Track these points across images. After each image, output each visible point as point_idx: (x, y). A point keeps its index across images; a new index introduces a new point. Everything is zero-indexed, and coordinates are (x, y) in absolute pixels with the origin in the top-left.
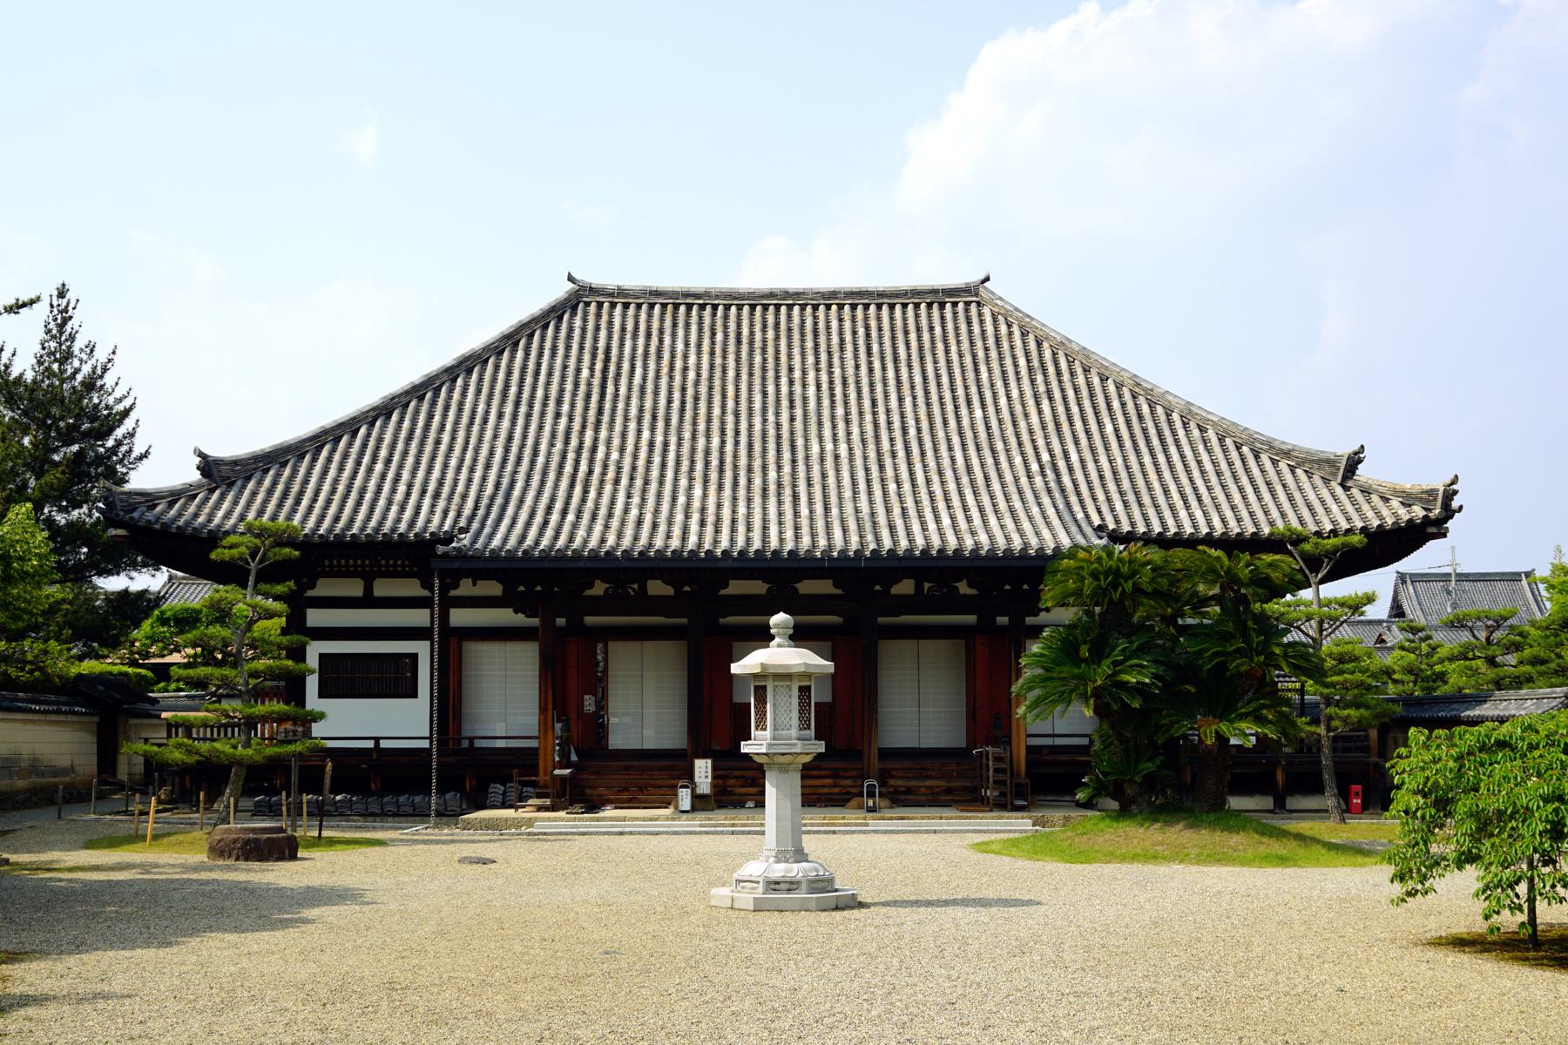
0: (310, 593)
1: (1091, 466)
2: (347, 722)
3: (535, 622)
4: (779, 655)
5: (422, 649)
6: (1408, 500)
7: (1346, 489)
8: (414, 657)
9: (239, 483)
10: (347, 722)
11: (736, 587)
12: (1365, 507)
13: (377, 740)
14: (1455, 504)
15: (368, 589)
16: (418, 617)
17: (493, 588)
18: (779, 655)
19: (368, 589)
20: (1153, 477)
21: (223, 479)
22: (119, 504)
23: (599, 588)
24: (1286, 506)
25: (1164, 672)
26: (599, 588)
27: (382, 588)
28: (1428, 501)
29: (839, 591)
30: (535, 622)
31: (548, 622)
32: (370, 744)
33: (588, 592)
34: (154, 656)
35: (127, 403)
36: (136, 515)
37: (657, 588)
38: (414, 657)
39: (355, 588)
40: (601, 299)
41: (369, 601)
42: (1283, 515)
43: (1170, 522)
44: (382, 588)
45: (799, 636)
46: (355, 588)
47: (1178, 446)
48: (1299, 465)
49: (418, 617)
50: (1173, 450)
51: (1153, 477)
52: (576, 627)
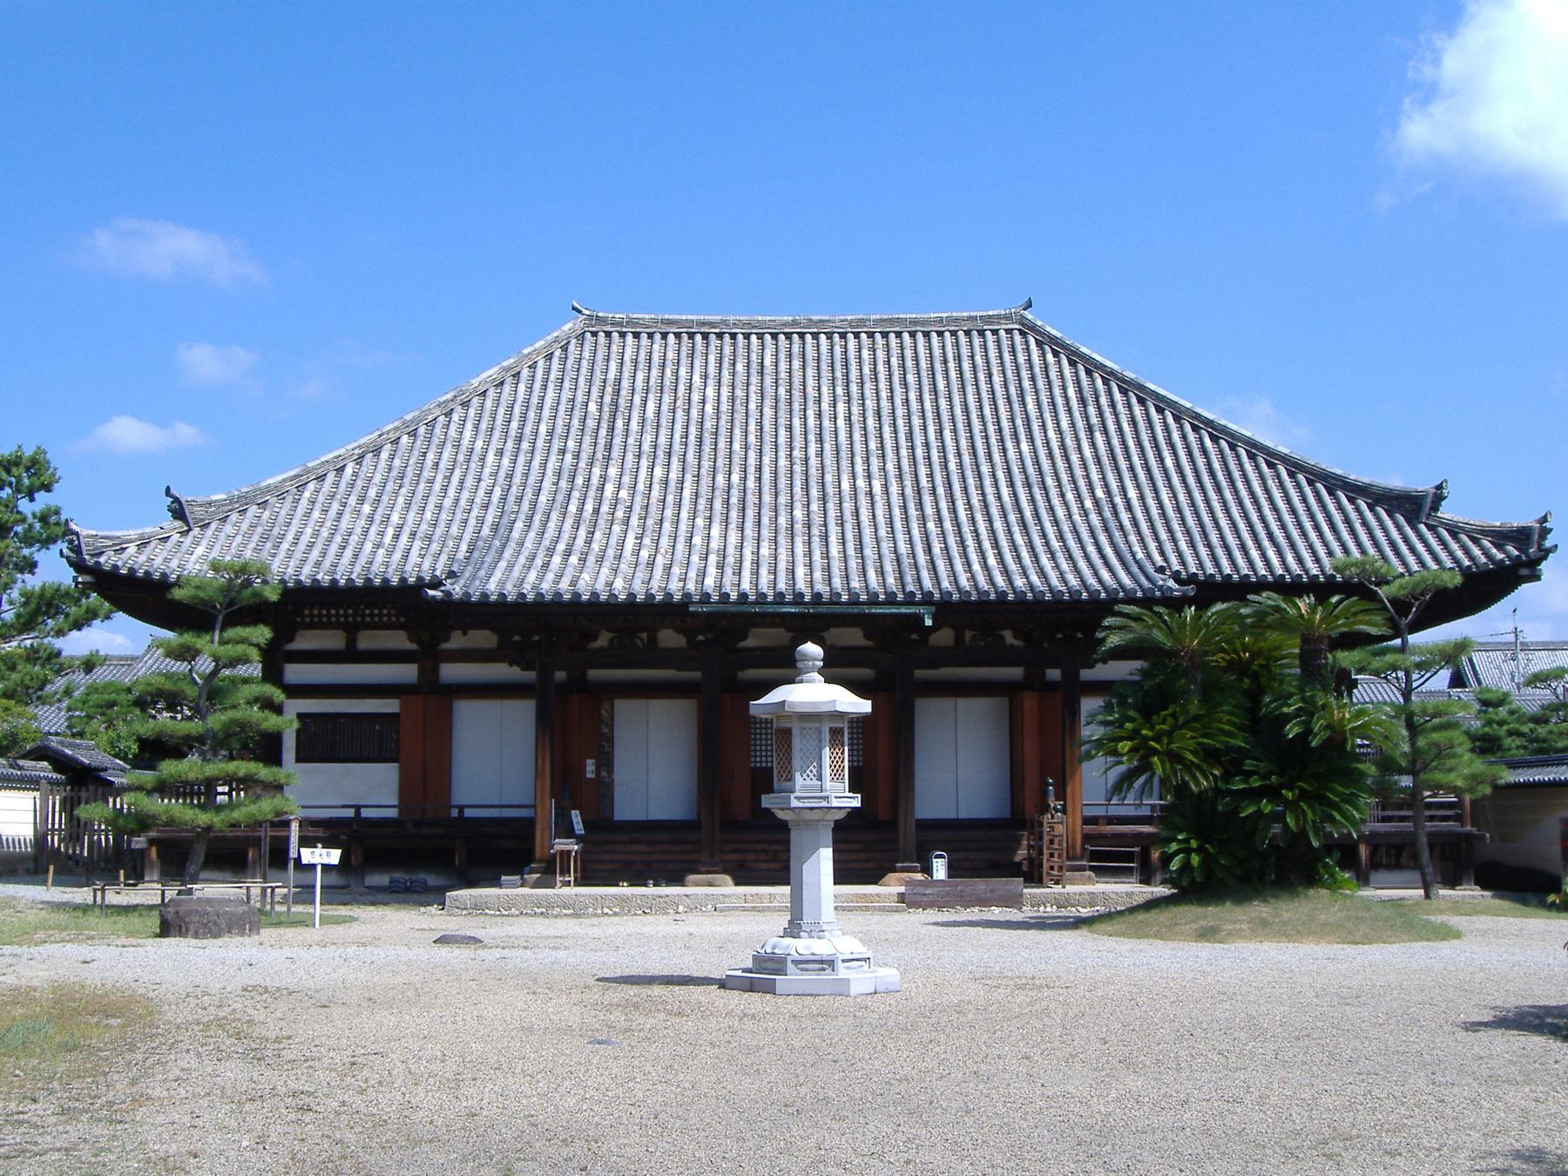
3: (531, 675)
4: (814, 692)
6: (1501, 537)
7: (1431, 528)
9: (213, 526)
12: (1454, 546)
13: (358, 808)
14: (1548, 544)
15: (351, 643)
16: (407, 672)
17: (484, 638)
18: (814, 692)
19: (351, 643)
27: (366, 641)
30: (531, 675)
31: (545, 675)
32: (350, 813)
39: (334, 640)
40: (608, 328)
43: (1241, 562)
44: (366, 641)
45: (834, 669)
49: (407, 672)
52: (579, 685)
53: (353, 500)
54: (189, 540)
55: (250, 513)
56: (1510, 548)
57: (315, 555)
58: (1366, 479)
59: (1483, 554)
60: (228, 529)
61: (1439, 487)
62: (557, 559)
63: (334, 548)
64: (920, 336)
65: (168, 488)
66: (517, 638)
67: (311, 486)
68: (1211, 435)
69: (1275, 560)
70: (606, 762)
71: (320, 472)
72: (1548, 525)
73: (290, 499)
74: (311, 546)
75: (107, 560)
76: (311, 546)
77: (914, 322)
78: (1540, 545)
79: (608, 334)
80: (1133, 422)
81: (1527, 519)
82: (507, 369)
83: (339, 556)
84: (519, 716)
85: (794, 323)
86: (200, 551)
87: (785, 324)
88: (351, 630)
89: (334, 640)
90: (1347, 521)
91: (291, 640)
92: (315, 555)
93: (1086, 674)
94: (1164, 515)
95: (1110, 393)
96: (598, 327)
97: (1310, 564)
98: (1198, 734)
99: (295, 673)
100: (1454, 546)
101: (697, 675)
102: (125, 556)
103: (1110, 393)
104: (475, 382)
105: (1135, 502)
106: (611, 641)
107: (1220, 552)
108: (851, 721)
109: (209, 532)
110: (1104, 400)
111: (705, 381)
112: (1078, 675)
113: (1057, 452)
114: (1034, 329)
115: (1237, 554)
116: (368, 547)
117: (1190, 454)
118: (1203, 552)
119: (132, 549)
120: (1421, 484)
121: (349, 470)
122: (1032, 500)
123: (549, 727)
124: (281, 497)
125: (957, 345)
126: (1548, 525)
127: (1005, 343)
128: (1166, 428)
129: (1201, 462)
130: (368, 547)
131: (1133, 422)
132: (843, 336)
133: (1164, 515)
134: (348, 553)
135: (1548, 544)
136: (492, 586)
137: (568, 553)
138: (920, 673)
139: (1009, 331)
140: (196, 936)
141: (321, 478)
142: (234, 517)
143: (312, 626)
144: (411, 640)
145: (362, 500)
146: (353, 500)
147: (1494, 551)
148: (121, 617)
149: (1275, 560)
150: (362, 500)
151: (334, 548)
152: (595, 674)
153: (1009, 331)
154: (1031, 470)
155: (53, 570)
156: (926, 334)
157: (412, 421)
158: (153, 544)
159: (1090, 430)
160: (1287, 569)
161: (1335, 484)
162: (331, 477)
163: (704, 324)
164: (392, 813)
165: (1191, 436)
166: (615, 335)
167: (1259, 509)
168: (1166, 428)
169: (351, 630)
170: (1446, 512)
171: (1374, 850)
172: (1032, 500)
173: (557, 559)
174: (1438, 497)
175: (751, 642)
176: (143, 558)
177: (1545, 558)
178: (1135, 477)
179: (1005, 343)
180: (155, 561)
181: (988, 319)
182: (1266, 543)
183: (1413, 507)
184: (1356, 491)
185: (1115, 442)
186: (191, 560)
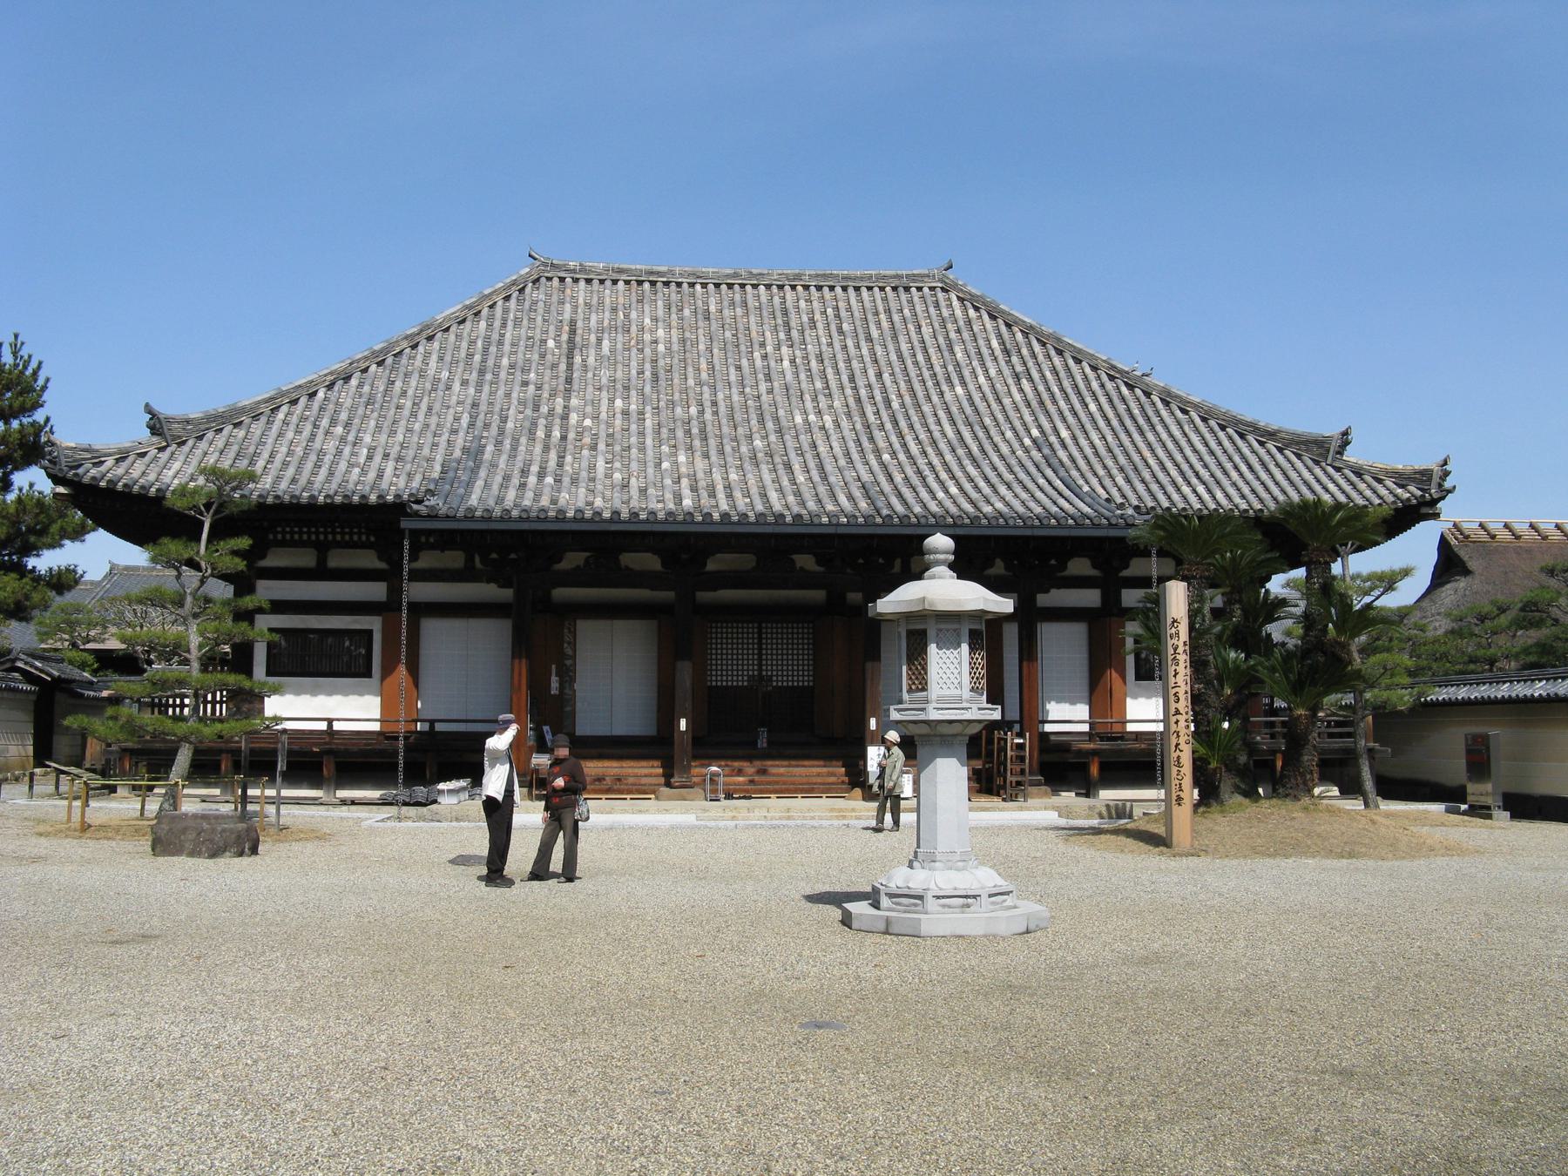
0: (1125, 573)
1: (1083, 442)
2: (297, 708)
3: (507, 594)
4: (944, 589)
5: (374, 623)
6: (1402, 479)
7: (1338, 470)
8: (369, 633)
9: (190, 443)
10: (297, 708)
12: (1362, 486)
13: (330, 721)
14: (1447, 484)
15: (322, 561)
16: (376, 591)
17: (453, 559)
19: (322, 561)
20: (1147, 454)
21: (174, 438)
22: (63, 460)
23: (572, 560)
24: (1284, 483)
25: (1262, 646)
26: (572, 560)
27: (336, 560)
28: (1422, 481)
29: (45, 562)
30: (507, 594)
32: (323, 726)
33: (558, 567)
34: (94, 640)
35: (34, 365)
36: (80, 471)
37: (806, 561)
38: (369, 633)
39: (306, 559)
40: (562, 274)
41: (321, 573)
42: (1284, 492)
43: (1175, 497)
44: (336, 560)
45: (967, 564)
46: (306, 559)
47: (1166, 427)
48: (1287, 446)
49: (376, 591)
50: (1159, 428)
51: (1147, 454)
53: (325, 423)
54: (164, 456)
55: (225, 432)
56: (1411, 488)
57: (291, 472)
58: (1274, 425)
59: (1389, 494)
60: (203, 445)
61: (1345, 433)
62: (532, 480)
63: (309, 465)
64: (851, 290)
65: (147, 405)
66: (494, 556)
67: (285, 409)
68: (1126, 384)
69: (1206, 496)
70: (568, 676)
71: (294, 396)
72: (1448, 468)
73: (263, 419)
74: (285, 464)
75: (90, 473)
76: (285, 464)
77: (846, 278)
78: (1440, 485)
79: (562, 280)
80: (1055, 371)
81: (1430, 462)
82: (469, 307)
83: (314, 474)
85: (736, 275)
86: (176, 465)
87: (728, 276)
88: (322, 549)
89: (305, 558)
90: (1263, 464)
91: (263, 557)
92: (291, 472)
93: (1043, 600)
94: (1097, 454)
95: (1029, 345)
96: (548, 273)
97: (1237, 500)
98: (1262, 646)
99: (267, 590)
100: (1362, 486)
102: (103, 469)
103: (1029, 345)
104: (440, 317)
105: (1069, 441)
106: (587, 560)
107: (1154, 487)
108: (988, 622)
109: (186, 448)
110: (1025, 351)
111: (657, 326)
112: (1035, 600)
113: (991, 398)
114: (955, 287)
115: (1170, 489)
116: (343, 466)
117: (1111, 401)
118: (1140, 487)
119: (110, 462)
120: (1329, 429)
121: (321, 394)
122: (976, 437)
123: (522, 644)
124: (256, 418)
125: (885, 299)
126: (1448, 468)
127: (930, 300)
128: (1086, 378)
129: (1121, 408)
130: (343, 466)
131: (1055, 371)
132: (781, 287)
133: (1097, 454)
134: (323, 472)
135: (1447, 484)
136: (474, 500)
137: (541, 475)
139: (932, 289)
140: (192, 854)
141: (294, 402)
142: (210, 435)
143: (283, 544)
144: (380, 558)
145: (333, 422)
146: (325, 423)
147: (1399, 491)
148: (101, 530)
149: (1206, 496)
150: (333, 422)
151: (309, 465)
152: (561, 593)
153: (932, 289)
154: (969, 410)
155: (33, 480)
156: (857, 289)
157: (381, 351)
158: (131, 459)
159: (1017, 377)
160: (1218, 503)
161: (1244, 429)
162: (303, 400)
163: (652, 273)
164: (376, 727)
165: (1109, 385)
166: (568, 280)
167: (1181, 451)
168: (1086, 378)
169: (322, 549)
170: (1351, 455)
171: (1104, 767)
172: (976, 437)
173: (532, 480)
174: (1345, 439)
175: (711, 566)
176: (120, 471)
177: (1443, 498)
178: (1064, 420)
179: (930, 300)
180: (140, 475)
181: (913, 277)
182: (1194, 481)
183: (1323, 450)
184: (1266, 435)
185: (1041, 388)
186: (174, 473)
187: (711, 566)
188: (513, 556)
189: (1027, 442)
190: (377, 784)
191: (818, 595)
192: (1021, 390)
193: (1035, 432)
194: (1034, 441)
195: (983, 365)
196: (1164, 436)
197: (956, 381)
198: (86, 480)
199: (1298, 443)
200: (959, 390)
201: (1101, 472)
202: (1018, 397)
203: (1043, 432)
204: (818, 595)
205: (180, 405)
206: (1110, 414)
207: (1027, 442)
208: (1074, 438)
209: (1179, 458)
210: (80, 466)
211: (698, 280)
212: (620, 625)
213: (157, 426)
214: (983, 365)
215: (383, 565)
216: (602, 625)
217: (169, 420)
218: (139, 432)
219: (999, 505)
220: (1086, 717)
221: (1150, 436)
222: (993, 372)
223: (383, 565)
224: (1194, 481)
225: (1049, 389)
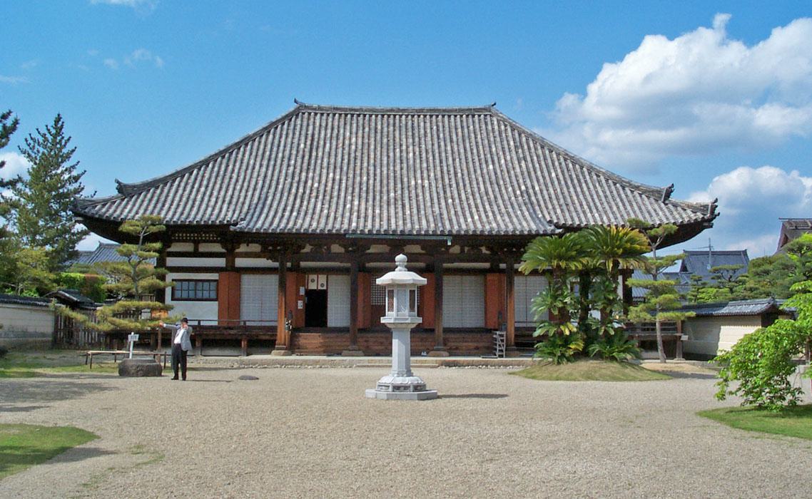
3: (276, 264)
11: (373, 249)
13: (199, 321)
14: (716, 212)
15: (196, 248)
16: (221, 262)
19: (196, 248)
27: (203, 248)
28: (703, 210)
29: (423, 252)
30: (276, 264)
36: (86, 210)
37: (336, 248)
39: (189, 247)
40: (310, 111)
41: (196, 254)
43: (583, 219)
44: (203, 248)
47: (587, 184)
49: (221, 262)
51: (575, 198)
52: (296, 269)
77: (444, 111)
79: (310, 114)
84: (273, 280)
88: (196, 243)
99: (171, 262)
101: (348, 265)
106: (312, 249)
115: (582, 215)
138: (445, 265)
143: (179, 241)
148: (92, 234)
149: (598, 219)
164: (215, 323)
169: (196, 243)
175: (372, 250)
177: (715, 218)
187: (372, 250)
188: (279, 248)
189: (518, 192)
190: (144, 349)
191: (487, 265)
192: (520, 167)
193: (523, 188)
194: (521, 192)
195: (504, 154)
196: (585, 189)
197: (490, 162)
198: (90, 214)
199: (649, 192)
200: (491, 167)
201: (550, 207)
202: (518, 170)
203: (527, 188)
204: (487, 265)
205: (133, 178)
206: (561, 178)
207: (518, 192)
208: (541, 190)
209: (590, 200)
210: (87, 208)
211: (374, 112)
212: (467, 279)
213: (122, 189)
214: (504, 154)
215: (224, 251)
216: (457, 278)
217: (125, 186)
218: (115, 193)
219: (494, 225)
220: (217, 319)
221: (578, 189)
222: (508, 158)
223: (224, 251)
224: (594, 211)
225: (281, 165)
